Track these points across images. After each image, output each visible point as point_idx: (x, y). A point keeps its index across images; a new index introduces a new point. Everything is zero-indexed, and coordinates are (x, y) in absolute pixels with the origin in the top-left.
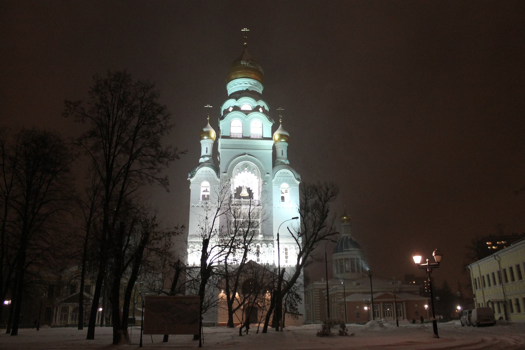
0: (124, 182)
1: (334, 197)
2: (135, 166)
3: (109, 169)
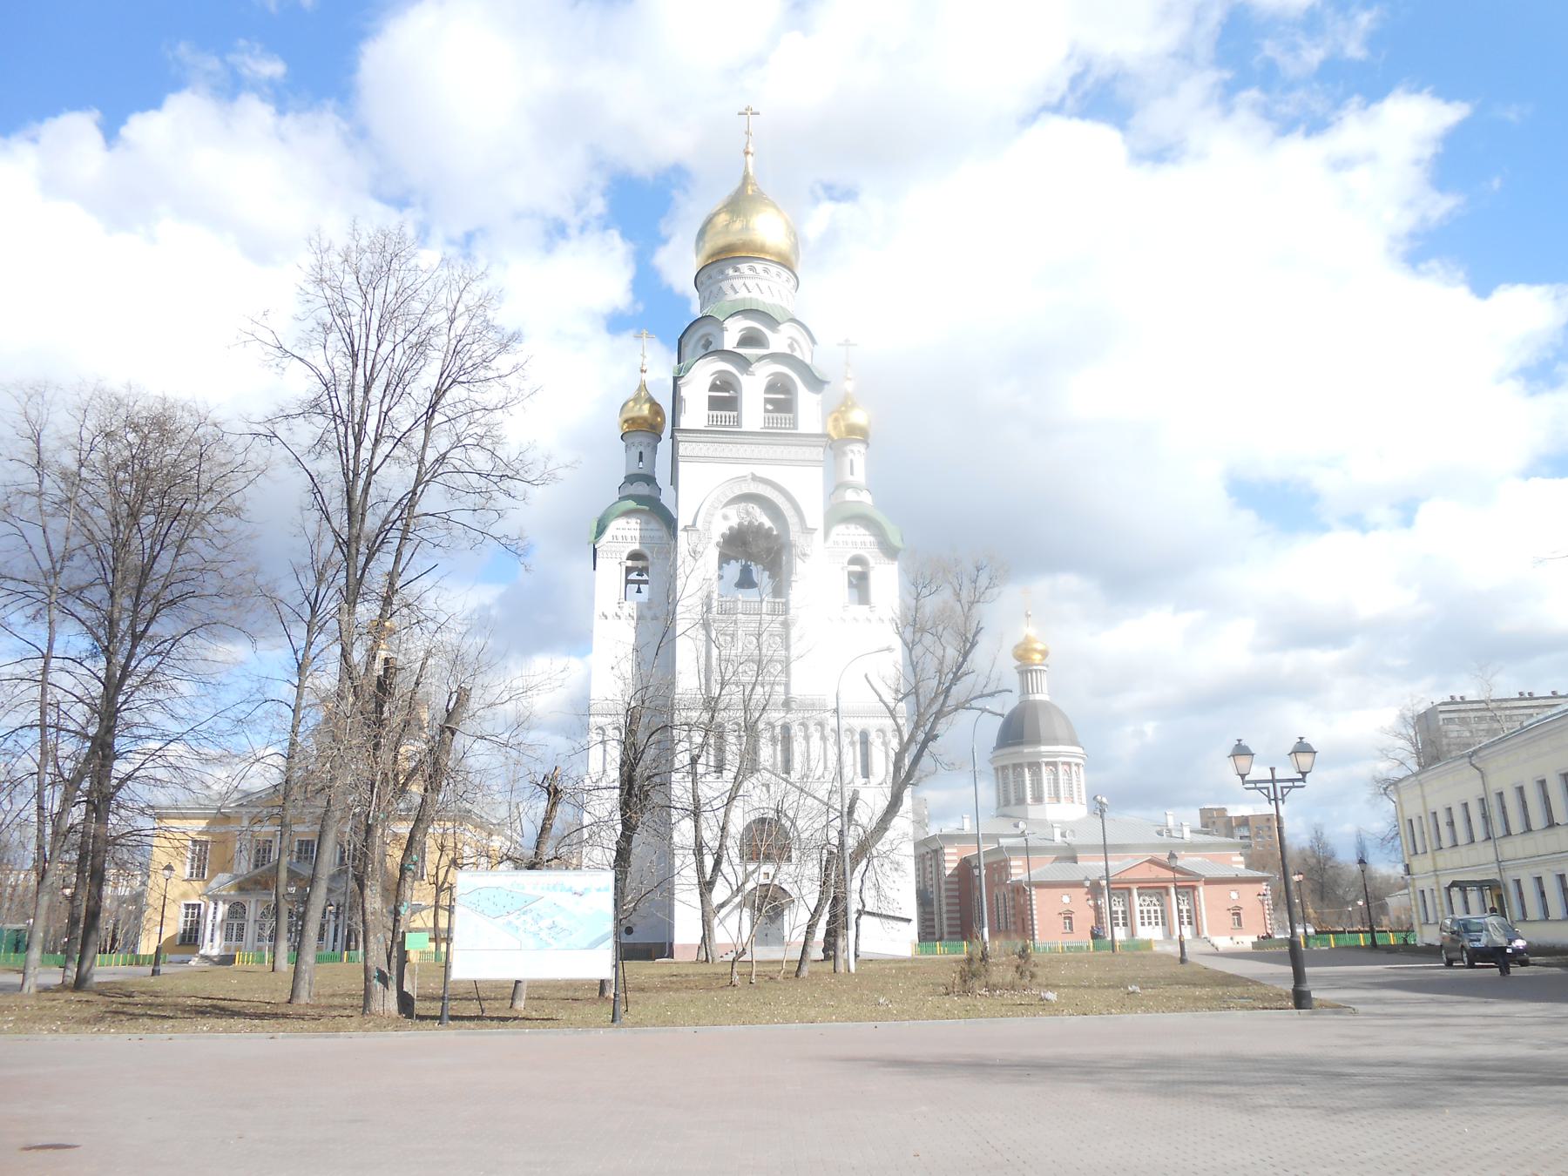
1: (996, 590)
3: (354, 513)
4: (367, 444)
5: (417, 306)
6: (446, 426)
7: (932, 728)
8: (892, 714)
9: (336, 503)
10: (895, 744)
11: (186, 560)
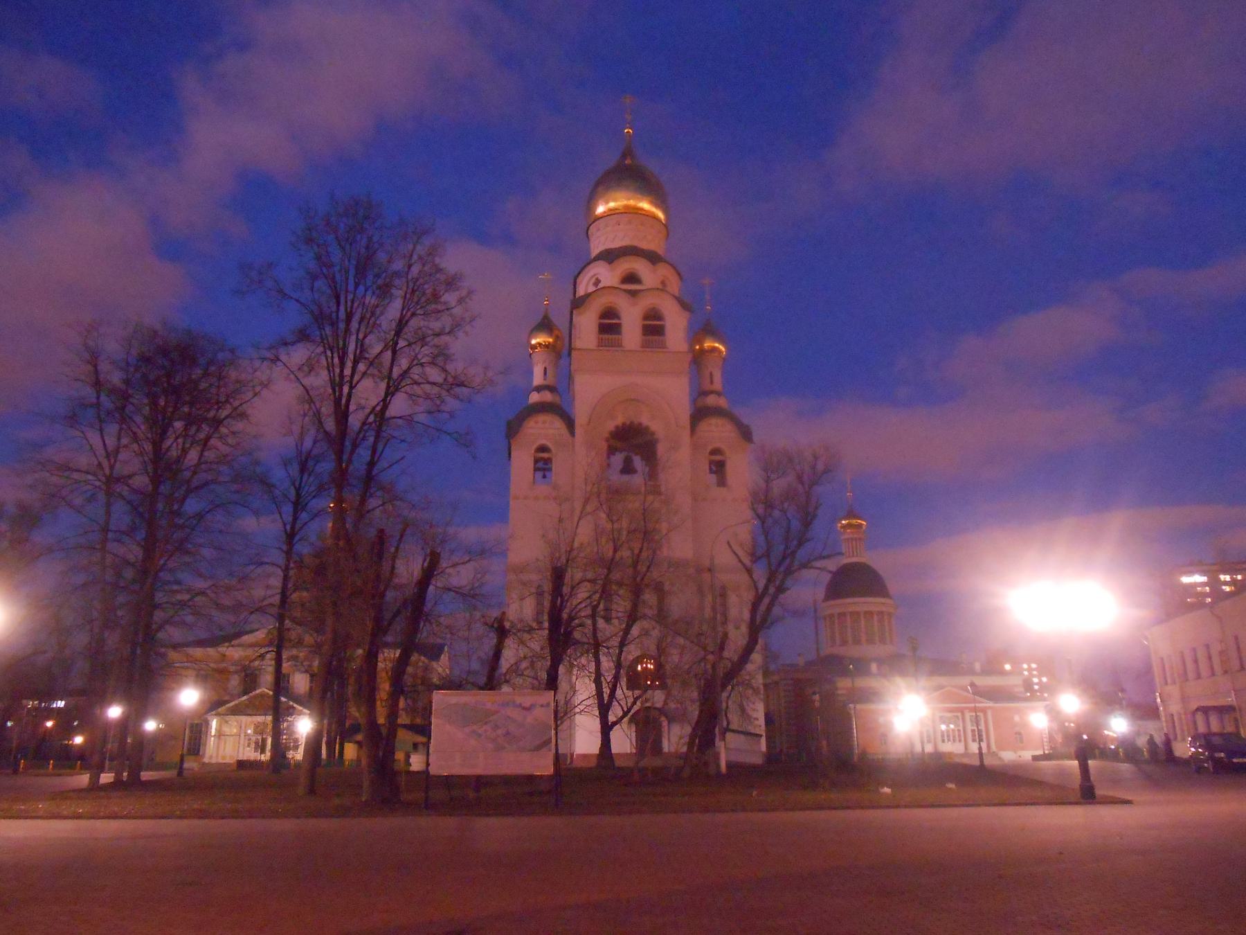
0: (375, 443)
2: (399, 406)
3: (342, 415)
4: (349, 364)
6: (407, 350)
7: (783, 581)
8: (749, 571)
9: (327, 409)
10: (749, 596)
11: (210, 455)
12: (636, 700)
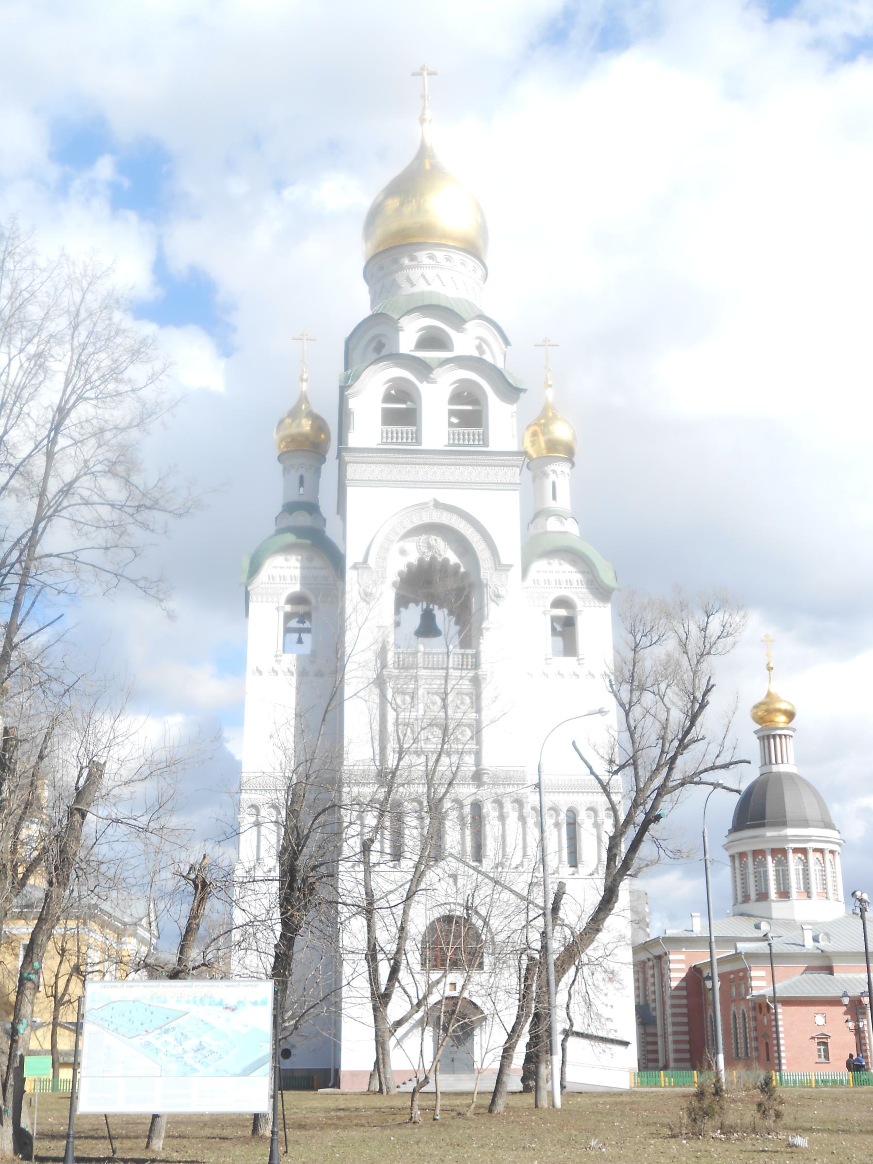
1: (730, 640)
5: (34, 311)
7: (654, 807)
8: (605, 789)
10: (609, 828)
12: (431, 987)
